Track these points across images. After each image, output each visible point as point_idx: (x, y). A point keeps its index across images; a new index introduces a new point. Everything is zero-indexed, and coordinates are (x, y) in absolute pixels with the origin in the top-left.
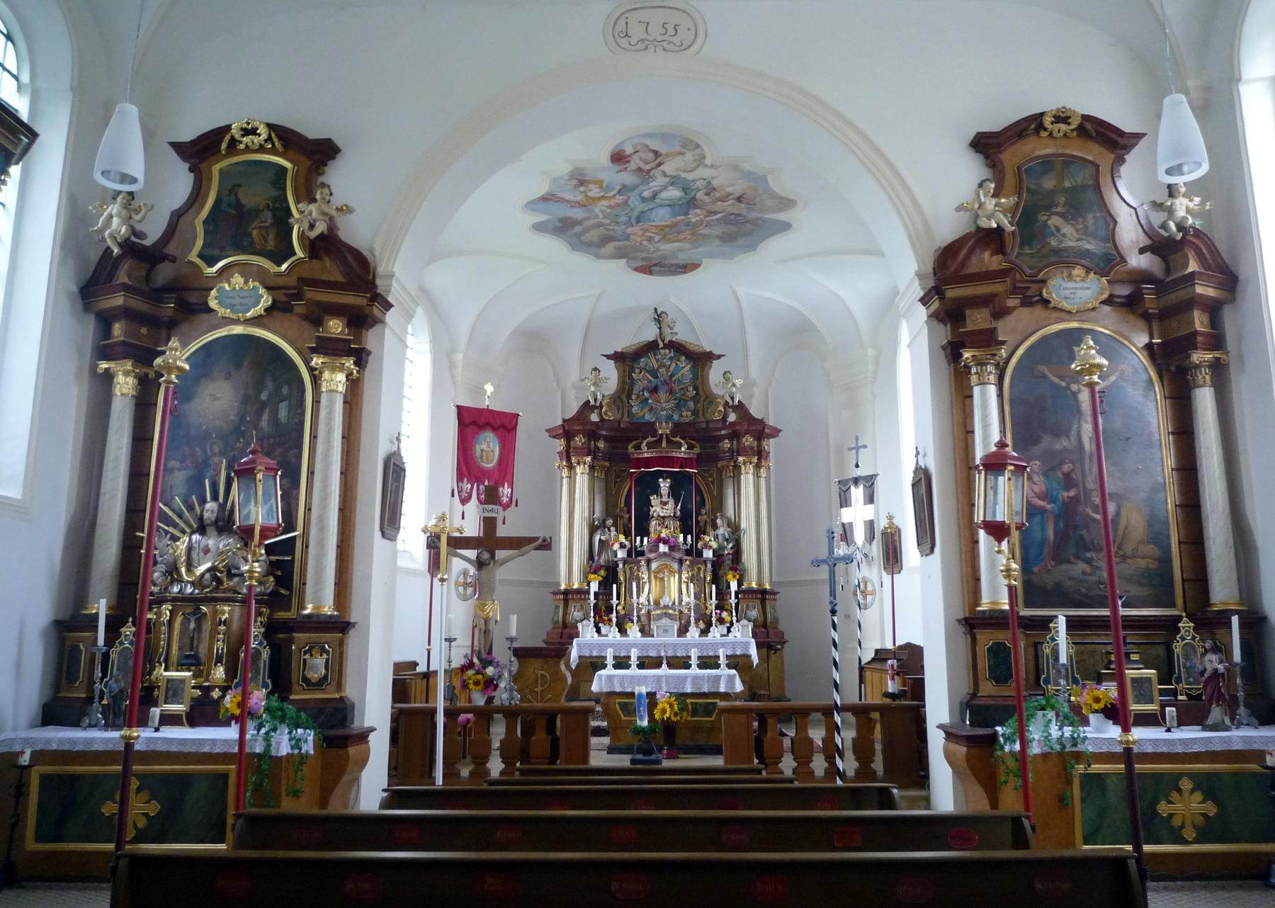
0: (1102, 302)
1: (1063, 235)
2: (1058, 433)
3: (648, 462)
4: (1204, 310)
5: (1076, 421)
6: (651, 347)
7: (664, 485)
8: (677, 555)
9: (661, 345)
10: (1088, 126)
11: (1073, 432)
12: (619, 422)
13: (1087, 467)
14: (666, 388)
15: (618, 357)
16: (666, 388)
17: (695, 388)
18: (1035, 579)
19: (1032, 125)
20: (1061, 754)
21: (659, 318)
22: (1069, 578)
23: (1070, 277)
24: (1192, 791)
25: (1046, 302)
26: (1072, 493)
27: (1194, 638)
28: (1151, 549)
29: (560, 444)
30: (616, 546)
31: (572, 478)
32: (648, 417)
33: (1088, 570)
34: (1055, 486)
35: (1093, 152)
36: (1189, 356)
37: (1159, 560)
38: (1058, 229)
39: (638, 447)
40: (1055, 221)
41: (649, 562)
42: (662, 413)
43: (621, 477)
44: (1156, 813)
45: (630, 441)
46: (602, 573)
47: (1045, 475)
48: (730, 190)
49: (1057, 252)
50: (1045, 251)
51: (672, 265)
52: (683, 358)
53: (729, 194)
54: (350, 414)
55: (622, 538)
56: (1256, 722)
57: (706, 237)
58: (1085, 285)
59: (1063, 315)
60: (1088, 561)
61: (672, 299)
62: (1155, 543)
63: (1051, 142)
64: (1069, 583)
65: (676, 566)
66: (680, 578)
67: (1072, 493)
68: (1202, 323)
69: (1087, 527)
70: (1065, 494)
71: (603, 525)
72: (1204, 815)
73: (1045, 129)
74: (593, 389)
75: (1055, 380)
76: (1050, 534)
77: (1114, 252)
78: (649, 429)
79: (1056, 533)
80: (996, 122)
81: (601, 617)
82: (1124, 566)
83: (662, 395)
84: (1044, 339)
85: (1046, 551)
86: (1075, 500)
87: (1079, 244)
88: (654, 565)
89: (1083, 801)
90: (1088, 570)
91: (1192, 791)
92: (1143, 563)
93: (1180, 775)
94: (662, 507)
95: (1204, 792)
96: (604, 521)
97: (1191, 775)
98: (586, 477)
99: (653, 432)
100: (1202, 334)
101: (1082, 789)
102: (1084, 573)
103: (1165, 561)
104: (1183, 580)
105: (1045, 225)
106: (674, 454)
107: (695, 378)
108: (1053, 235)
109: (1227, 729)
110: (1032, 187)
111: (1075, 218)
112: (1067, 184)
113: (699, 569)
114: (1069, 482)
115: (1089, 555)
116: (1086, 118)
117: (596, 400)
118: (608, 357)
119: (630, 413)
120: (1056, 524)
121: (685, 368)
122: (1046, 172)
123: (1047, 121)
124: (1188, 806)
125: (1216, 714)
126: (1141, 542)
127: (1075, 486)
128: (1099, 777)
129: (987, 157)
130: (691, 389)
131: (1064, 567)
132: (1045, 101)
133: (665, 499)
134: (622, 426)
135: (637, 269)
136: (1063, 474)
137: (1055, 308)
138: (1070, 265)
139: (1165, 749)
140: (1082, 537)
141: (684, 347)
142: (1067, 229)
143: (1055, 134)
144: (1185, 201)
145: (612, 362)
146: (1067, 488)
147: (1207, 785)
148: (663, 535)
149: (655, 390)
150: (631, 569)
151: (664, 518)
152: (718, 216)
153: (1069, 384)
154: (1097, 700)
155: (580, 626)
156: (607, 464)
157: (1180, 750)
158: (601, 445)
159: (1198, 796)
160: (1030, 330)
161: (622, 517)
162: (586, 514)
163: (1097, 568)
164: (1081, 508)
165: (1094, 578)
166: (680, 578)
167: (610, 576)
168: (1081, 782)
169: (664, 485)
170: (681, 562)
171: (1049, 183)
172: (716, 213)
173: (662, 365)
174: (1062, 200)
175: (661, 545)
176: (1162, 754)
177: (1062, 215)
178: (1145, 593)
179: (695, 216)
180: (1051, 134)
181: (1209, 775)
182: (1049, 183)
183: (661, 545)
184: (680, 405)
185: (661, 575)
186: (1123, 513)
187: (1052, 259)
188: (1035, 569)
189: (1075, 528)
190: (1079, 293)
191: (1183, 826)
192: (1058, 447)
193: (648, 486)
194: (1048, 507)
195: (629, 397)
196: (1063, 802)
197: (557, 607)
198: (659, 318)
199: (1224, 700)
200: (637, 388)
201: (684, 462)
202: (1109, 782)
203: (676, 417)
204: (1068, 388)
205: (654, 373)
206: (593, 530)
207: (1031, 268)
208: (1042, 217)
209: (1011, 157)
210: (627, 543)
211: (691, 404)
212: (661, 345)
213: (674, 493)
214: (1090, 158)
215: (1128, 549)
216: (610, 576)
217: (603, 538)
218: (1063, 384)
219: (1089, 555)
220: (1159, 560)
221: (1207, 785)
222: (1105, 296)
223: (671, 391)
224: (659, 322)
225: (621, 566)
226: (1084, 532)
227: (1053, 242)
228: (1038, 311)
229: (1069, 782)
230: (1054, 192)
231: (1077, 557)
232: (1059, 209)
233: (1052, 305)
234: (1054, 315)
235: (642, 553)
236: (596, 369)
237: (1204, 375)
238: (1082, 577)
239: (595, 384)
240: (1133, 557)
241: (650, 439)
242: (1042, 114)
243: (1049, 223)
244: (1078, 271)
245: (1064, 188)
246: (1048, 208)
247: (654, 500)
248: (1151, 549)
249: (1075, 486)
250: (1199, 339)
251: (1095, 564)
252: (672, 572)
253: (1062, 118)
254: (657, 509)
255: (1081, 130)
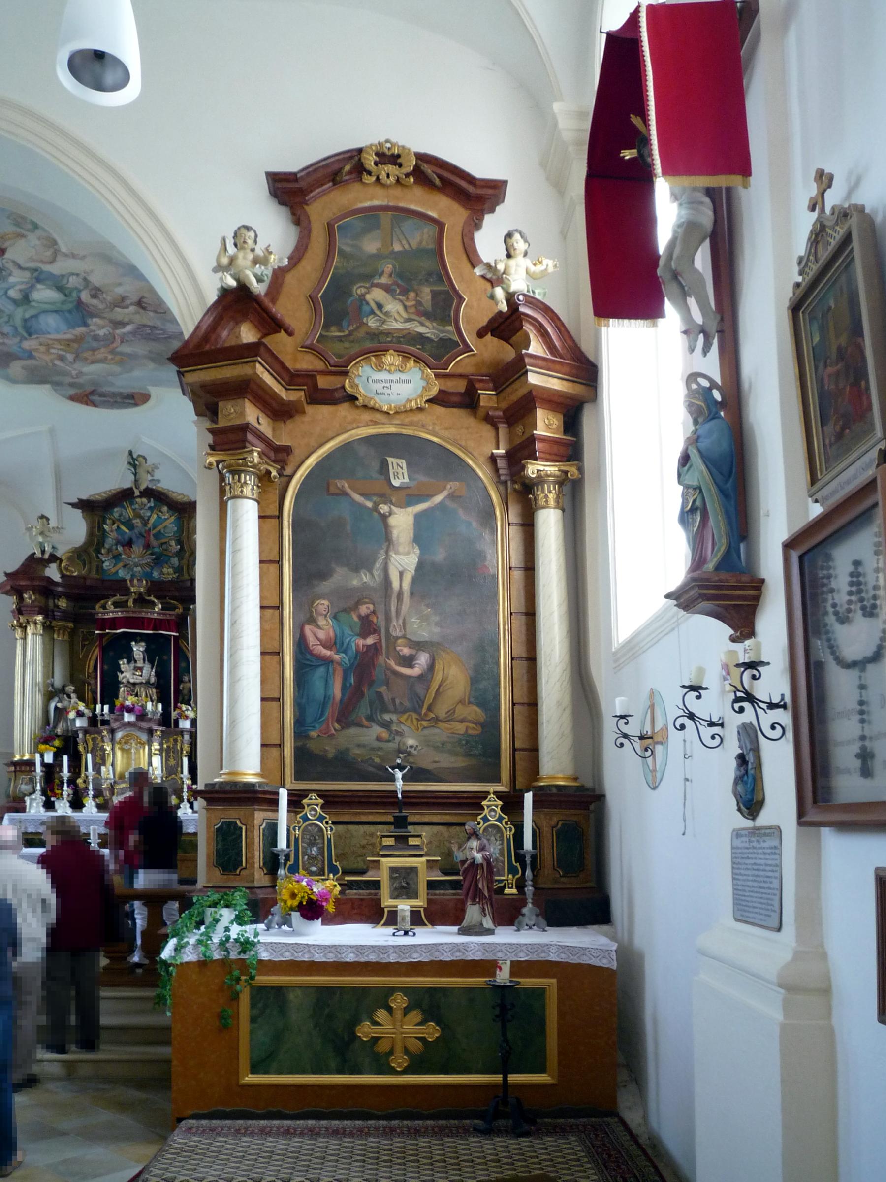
0: (428, 401)
1: (387, 314)
2: (362, 564)
3: (114, 623)
4: (553, 410)
5: (382, 552)
6: (125, 495)
7: (138, 649)
8: (145, 725)
9: (137, 493)
10: (428, 169)
11: (378, 565)
12: (85, 578)
13: (393, 609)
14: (141, 541)
15: (86, 506)
16: (141, 541)
17: (179, 542)
18: (311, 745)
19: (347, 168)
20: (224, 963)
21: (134, 462)
22: (359, 746)
23: (380, 367)
24: (406, 1011)
25: (353, 399)
26: (370, 641)
27: (500, 819)
28: (475, 712)
29: (11, 602)
30: (72, 715)
31: (25, 639)
32: (122, 574)
33: (385, 735)
34: (348, 631)
35: (439, 206)
36: (524, 468)
37: (483, 725)
38: (380, 306)
39: (104, 607)
40: (376, 295)
41: (112, 732)
42: (131, 568)
43: (88, 638)
44: (354, 1037)
45: (98, 600)
46: (57, 743)
47: (335, 617)
48: (119, 290)
49: (374, 335)
50: (361, 333)
51: (114, 395)
52: (165, 509)
53: (123, 299)
54: (579, 652)
55: (81, 707)
56: (543, 922)
57: (132, 356)
58: (403, 377)
59: (378, 416)
60: (386, 725)
61: (144, 439)
62: (479, 705)
63: (379, 191)
64: (357, 751)
65: (144, 737)
66: (150, 749)
67: (370, 641)
68: (548, 426)
69: (387, 683)
70: (361, 642)
71: (61, 692)
72: (423, 1040)
73: (369, 173)
74: (41, 539)
75: (358, 498)
76: (337, 691)
77: (456, 338)
78: (121, 587)
79: (344, 688)
80: (294, 162)
81: (52, 791)
82: (436, 731)
83: (137, 549)
84: (346, 448)
85: (328, 712)
86: (375, 649)
87: (407, 325)
88: (119, 735)
89: (253, 1020)
90: (385, 735)
91: (406, 1011)
92: (461, 728)
93: (391, 991)
94: (136, 671)
95: (424, 1011)
96: (64, 687)
97: (406, 991)
98: (39, 639)
99: (126, 592)
100: (544, 439)
101: (253, 1006)
102: (379, 739)
103: (492, 725)
104: (514, 750)
105: (362, 299)
106: (143, 615)
107: (181, 530)
108: (372, 312)
109: (490, 932)
110: (347, 249)
111: (405, 292)
112: (397, 247)
113: (176, 741)
114: (367, 626)
115: (387, 717)
116: (422, 158)
117: (43, 552)
118: (74, 505)
119: (100, 569)
120: (345, 679)
121: (168, 521)
122: (367, 230)
123: (370, 160)
124: (397, 1028)
125: (473, 913)
126: (461, 702)
127: (376, 631)
128: (279, 991)
129: (293, 214)
130: (173, 543)
131: (353, 731)
132: (364, 133)
133: (140, 664)
134: (88, 582)
135: (72, 398)
136: (360, 617)
137: (365, 407)
138: (379, 351)
139: (373, 958)
140: (379, 695)
141: (167, 496)
142: (393, 306)
143: (383, 176)
144: (526, 263)
145: (78, 513)
146: (364, 635)
147: (428, 1003)
148: (128, 703)
149: (129, 543)
150: (93, 739)
151: (134, 684)
152: (128, 328)
153: (376, 505)
154: (293, 896)
155: (27, 799)
156: (71, 625)
157: (393, 959)
158: (63, 603)
159: (416, 1016)
160: (330, 437)
161: (89, 684)
162: (39, 678)
163: (398, 733)
164: (381, 659)
165: (392, 746)
166: (150, 749)
167: (69, 746)
168: (252, 998)
169: (138, 649)
170: (151, 732)
171: (371, 245)
172: (122, 324)
173: (137, 515)
174: (388, 268)
175: (126, 714)
176: (367, 964)
177: (387, 289)
178: (463, 764)
179: (99, 327)
180: (378, 179)
181: (432, 991)
182: (371, 245)
183: (126, 714)
184: (159, 560)
185: (126, 747)
186: (439, 667)
187: (369, 345)
188: (313, 734)
189: (371, 683)
190: (396, 388)
191: (391, 1052)
192: (355, 582)
193: (118, 649)
194: (337, 657)
195: (98, 551)
196: (225, 1023)
197: (10, 779)
198: (134, 462)
199: (482, 897)
200: (109, 542)
201: (157, 624)
202: (291, 996)
203: (156, 574)
204: (375, 509)
205: (129, 524)
206: (49, 695)
207: (339, 356)
208: (358, 290)
209: (323, 207)
210: (87, 712)
211: (175, 561)
212: (137, 493)
213: (150, 655)
214: (433, 214)
215: (441, 710)
216: (69, 746)
217: (59, 705)
218: (369, 504)
219: (387, 717)
220: (483, 725)
221: (428, 1003)
222: (434, 391)
223: (147, 546)
224: (135, 466)
225: (81, 736)
226: (383, 689)
227: (372, 323)
228: (344, 410)
229: (235, 997)
230: (378, 257)
231: (370, 718)
232: (384, 280)
233: (360, 402)
234: (366, 416)
235: (105, 723)
236: (42, 517)
237: (549, 494)
238: (377, 744)
239: (42, 533)
240: (448, 720)
241: (118, 598)
242: (360, 151)
243: (368, 297)
244: (391, 358)
245: (393, 252)
246: (368, 278)
247: (123, 663)
248: (475, 712)
249: (376, 631)
250: (538, 445)
251: (394, 728)
252: (142, 744)
253: (389, 157)
254: (127, 673)
255: (417, 173)
